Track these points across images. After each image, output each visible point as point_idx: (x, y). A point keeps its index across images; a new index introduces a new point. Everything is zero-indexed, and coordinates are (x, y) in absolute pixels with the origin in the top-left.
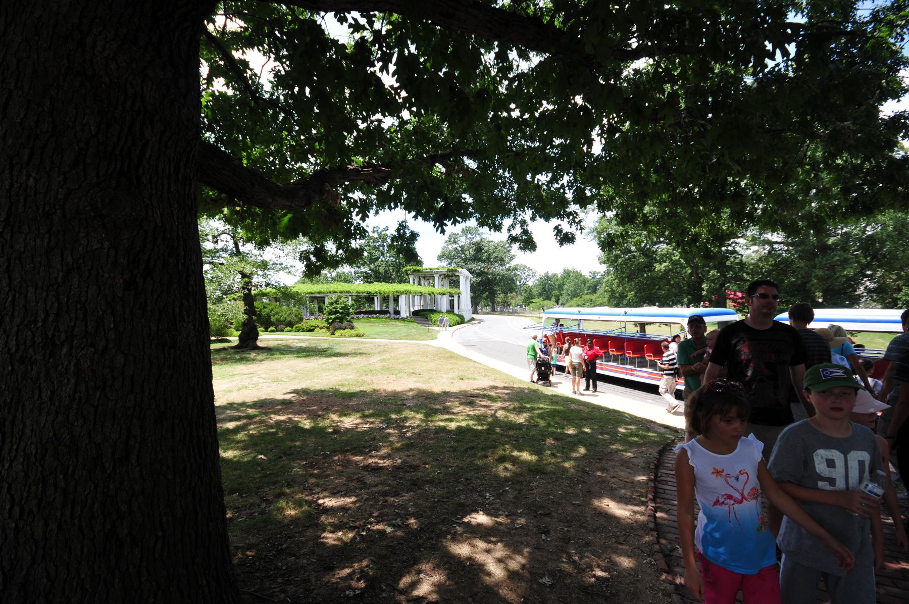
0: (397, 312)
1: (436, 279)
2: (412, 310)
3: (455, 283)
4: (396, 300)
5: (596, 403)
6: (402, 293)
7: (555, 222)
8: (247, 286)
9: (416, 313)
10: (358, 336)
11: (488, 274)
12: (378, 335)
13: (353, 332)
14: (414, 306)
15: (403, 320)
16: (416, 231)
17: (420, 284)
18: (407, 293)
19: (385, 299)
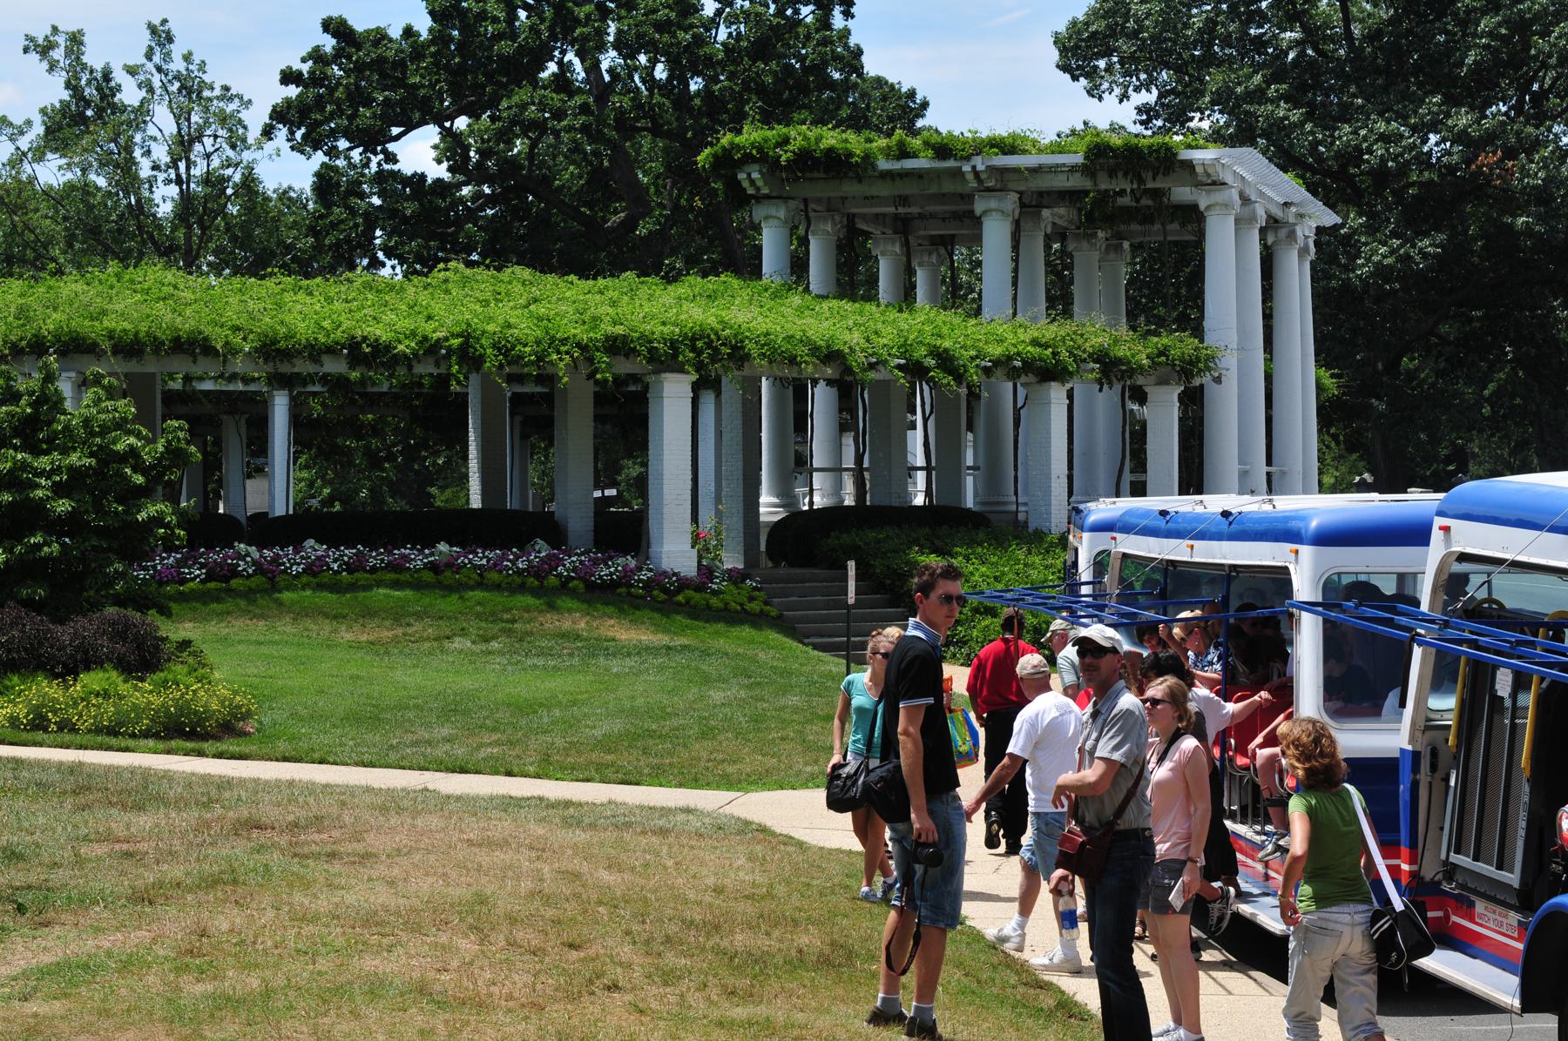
0: (625, 530)
1: (996, 234)
2: (769, 507)
3: (1169, 288)
4: (625, 421)
5: (969, 855)
6: (666, 357)
7: (39, 129)
8: (954, 278)
9: (804, 541)
10: (183, 730)
11: (1511, 201)
12: (376, 732)
13: (143, 695)
14: (797, 465)
15: (669, 599)
16: (73, 28)
17: (853, 281)
18: (714, 361)
19: (532, 407)
